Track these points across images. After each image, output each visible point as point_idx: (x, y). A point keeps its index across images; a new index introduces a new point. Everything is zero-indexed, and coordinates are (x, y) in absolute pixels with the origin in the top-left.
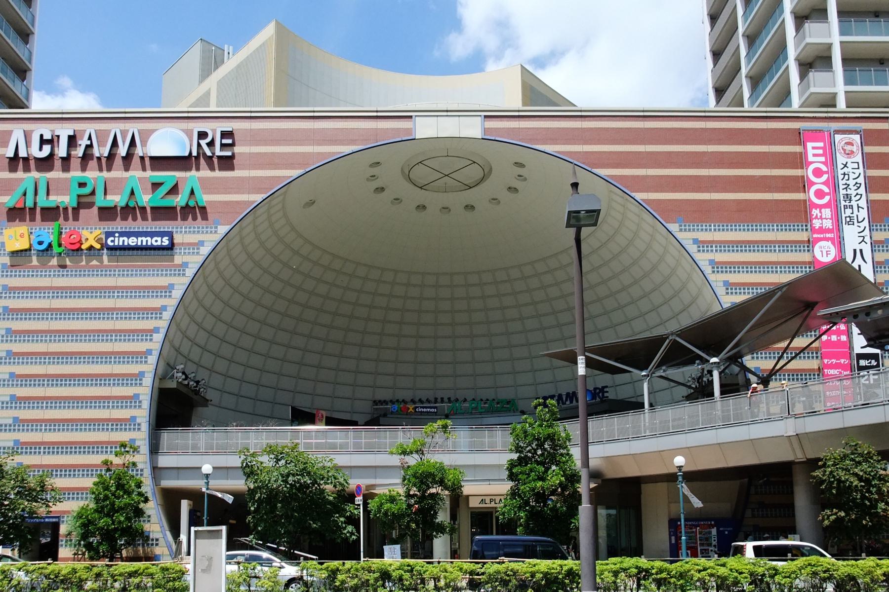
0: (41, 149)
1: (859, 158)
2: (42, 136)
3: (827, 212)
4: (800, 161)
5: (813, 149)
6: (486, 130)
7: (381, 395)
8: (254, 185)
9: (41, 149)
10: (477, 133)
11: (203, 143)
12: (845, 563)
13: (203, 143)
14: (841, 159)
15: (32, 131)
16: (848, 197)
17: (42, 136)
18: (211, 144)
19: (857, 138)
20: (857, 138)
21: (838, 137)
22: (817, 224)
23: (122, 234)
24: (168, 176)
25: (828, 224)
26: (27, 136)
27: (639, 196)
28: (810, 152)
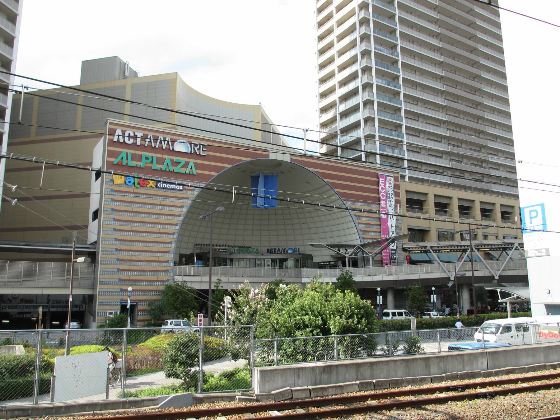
0: (129, 140)
1: (392, 185)
2: (129, 134)
3: (384, 202)
4: (378, 184)
5: (381, 180)
6: (292, 160)
7: (199, 241)
8: (214, 169)
9: (129, 140)
10: (289, 161)
11: (196, 148)
12: (107, 411)
13: (196, 148)
14: (388, 185)
15: (125, 131)
16: (389, 198)
17: (129, 134)
18: (199, 149)
19: (392, 178)
20: (392, 178)
21: (388, 177)
22: (382, 205)
23: (164, 182)
24: (183, 160)
25: (385, 206)
26: (124, 132)
27: (326, 180)
28: (381, 182)
